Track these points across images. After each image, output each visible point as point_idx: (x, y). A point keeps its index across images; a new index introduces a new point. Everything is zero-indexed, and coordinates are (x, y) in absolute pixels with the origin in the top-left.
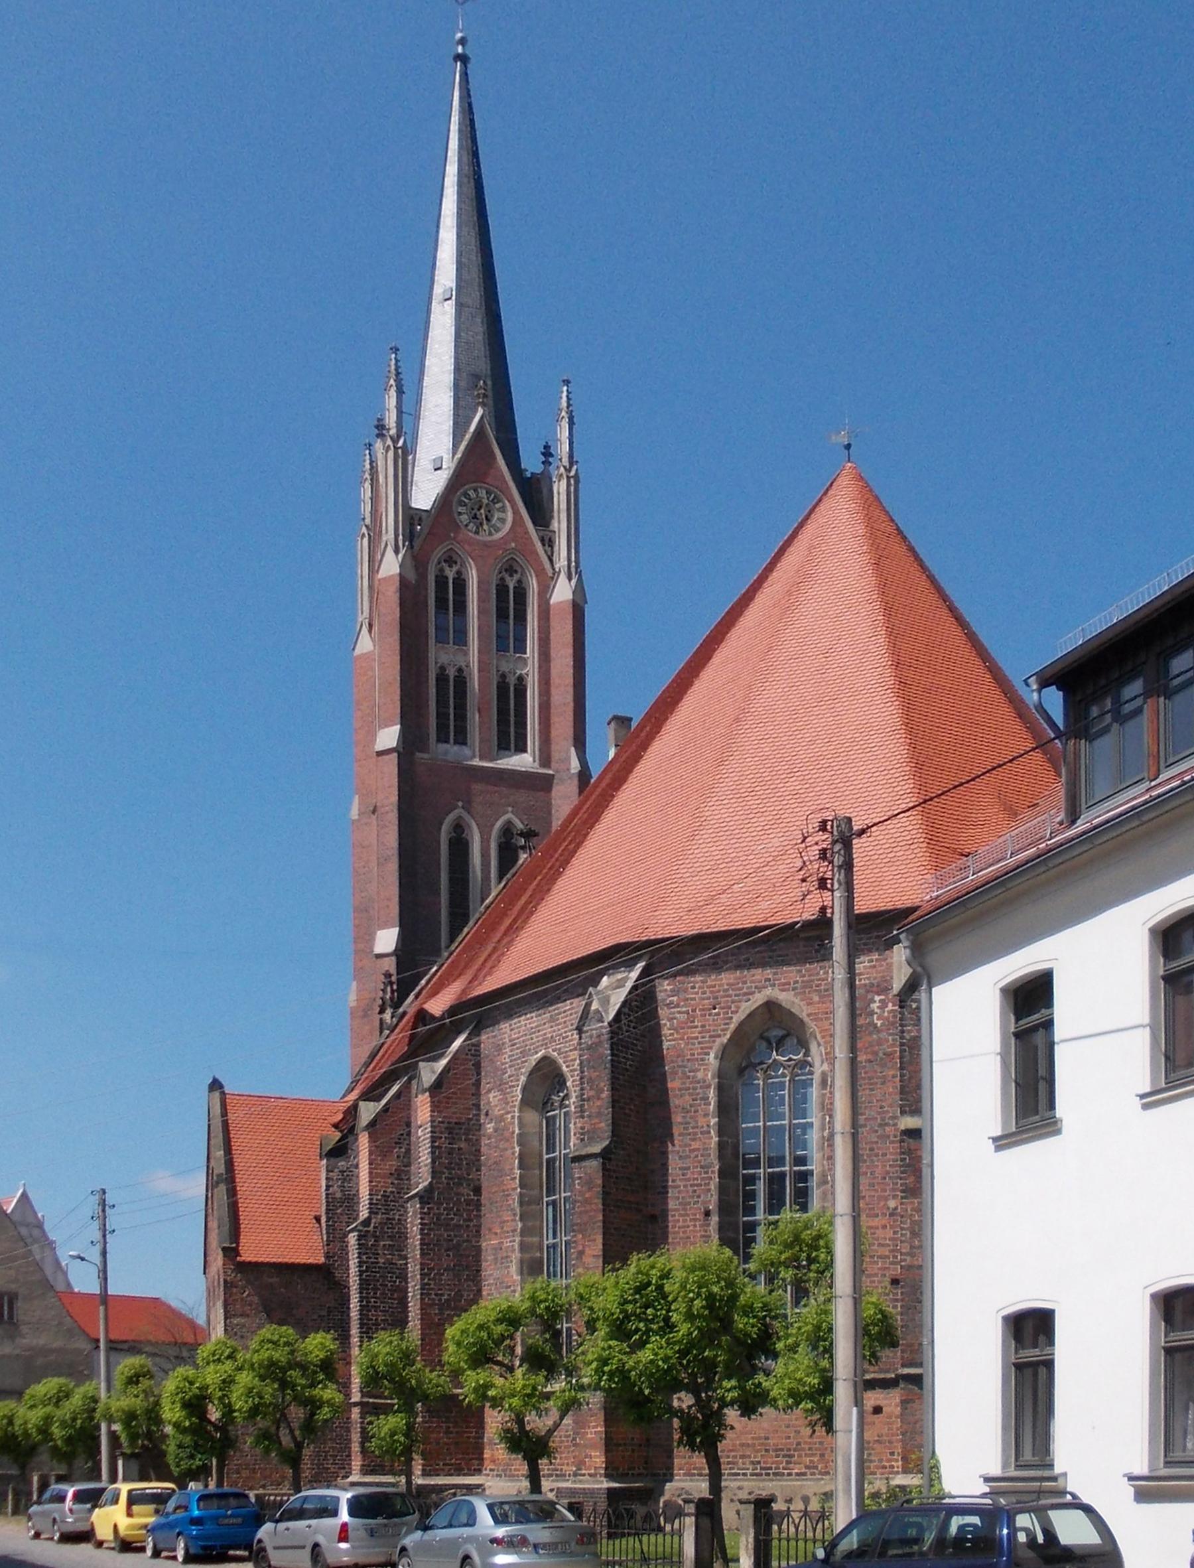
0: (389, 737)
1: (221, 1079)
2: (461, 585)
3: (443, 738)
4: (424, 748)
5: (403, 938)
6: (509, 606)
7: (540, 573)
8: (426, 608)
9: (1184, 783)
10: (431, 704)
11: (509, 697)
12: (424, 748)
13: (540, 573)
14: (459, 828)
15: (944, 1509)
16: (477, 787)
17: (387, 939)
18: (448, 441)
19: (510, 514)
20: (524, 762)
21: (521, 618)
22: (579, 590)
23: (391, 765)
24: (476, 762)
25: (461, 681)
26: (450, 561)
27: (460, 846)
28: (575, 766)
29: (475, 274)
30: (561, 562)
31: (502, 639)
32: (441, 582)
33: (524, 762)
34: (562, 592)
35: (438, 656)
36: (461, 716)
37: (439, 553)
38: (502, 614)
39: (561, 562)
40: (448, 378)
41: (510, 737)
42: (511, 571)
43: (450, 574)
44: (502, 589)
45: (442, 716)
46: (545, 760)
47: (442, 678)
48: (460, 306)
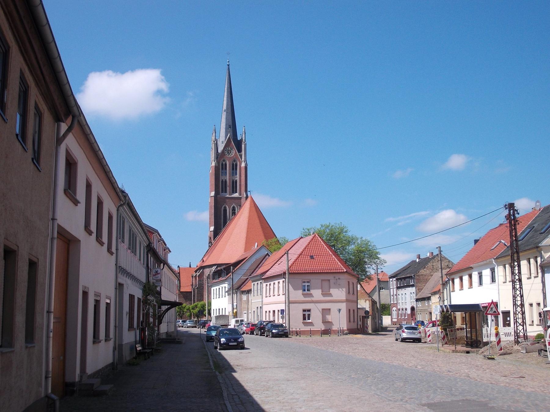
0: (213, 194)
1: (87, 286)
2: (226, 165)
3: (222, 192)
4: (219, 194)
5: (215, 228)
6: (234, 167)
7: (240, 161)
8: (219, 170)
9: (49, 312)
10: (220, 186)
11: (234, 183)
12: (219, 194)
13: (240, 161)
14: (225, 207)
15: (231, 266)
16: (227, 200)
17: (212, 228)
18: (224, 138)
19: (234, 152)
20: (236, 195)
21: (236, 169)
22: (246, 165)
23: (213, 198)
24: (228, 196)
25: (226, 181)
26: (224, 161)
27: (225, 210)
28: (245, 195)
29: (230, 106)
30: (243, 159)
31: (233, 173)
32: (222, 164)
33: (236, 195)
34: (243, 165)
35: (222, 178)
36: (226, 188)
37: (222, 160)
38: (233, 169)
39: (243, 159)
40: (224, 127)
41: (234, 191)
42: (235, 161)
43: (224, 163)
44: (233, 164)
45: (222, 188)
46: (240, 195)
47: (222, 181)
48: (227, 113)
